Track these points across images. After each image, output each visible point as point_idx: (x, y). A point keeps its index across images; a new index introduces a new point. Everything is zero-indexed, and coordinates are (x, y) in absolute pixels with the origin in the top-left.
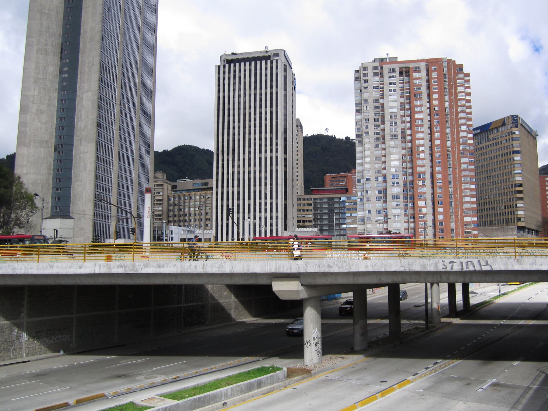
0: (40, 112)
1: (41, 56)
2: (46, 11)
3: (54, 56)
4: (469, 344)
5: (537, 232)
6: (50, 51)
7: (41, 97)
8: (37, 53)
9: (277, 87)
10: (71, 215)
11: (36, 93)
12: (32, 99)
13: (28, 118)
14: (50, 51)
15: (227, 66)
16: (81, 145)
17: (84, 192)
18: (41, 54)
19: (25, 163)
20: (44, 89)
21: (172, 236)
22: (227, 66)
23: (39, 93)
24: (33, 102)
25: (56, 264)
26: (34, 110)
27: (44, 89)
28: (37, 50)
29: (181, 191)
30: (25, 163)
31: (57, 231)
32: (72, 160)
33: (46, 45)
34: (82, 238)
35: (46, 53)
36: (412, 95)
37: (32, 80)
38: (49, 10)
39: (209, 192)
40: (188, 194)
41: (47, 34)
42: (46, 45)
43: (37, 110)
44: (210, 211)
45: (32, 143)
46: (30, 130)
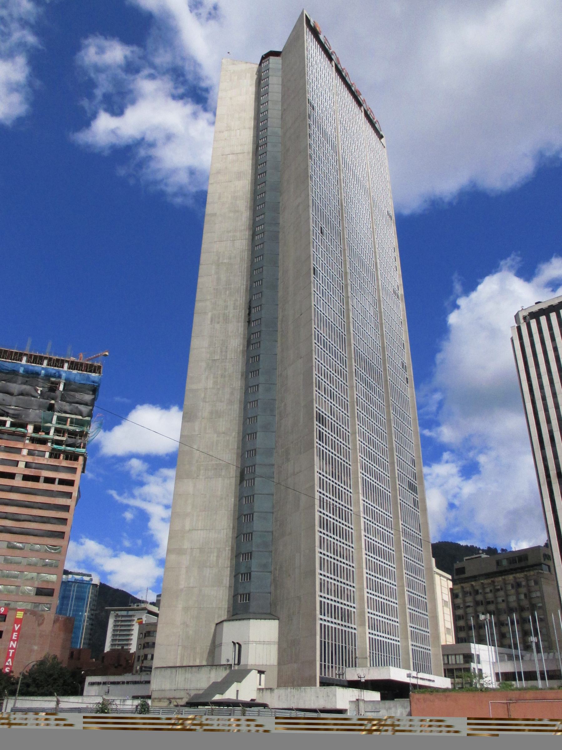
0: (216, 414)
1: (217, 326)
2: (225, 261)
3: (238, 322)
6: (231, 315)
7: (219, 389)
8: (212, 321)
9: (338, 730)
11: (210, 384)
12: (203, 395)
13: (197, 428)
14: (231, 315)
15: (533, 323)
18: (218, 323)
19: (189, 509)
20: (223, 376)
21: (480, 666)
23: (215, 383)
24: (204, 400)
26: (206, 414)
27: (223, 376)
29: (474, 578)
30: (189, 509)
31: (240, 646)
33: (226, 307)
34: (295, 666)
35: (226, 320)
37: (203, 364)
39: (532, 573)
40: (489, 581)
41: (227, 292)
42: (226, 307)
43: (211, 413)
45: (202, 472)
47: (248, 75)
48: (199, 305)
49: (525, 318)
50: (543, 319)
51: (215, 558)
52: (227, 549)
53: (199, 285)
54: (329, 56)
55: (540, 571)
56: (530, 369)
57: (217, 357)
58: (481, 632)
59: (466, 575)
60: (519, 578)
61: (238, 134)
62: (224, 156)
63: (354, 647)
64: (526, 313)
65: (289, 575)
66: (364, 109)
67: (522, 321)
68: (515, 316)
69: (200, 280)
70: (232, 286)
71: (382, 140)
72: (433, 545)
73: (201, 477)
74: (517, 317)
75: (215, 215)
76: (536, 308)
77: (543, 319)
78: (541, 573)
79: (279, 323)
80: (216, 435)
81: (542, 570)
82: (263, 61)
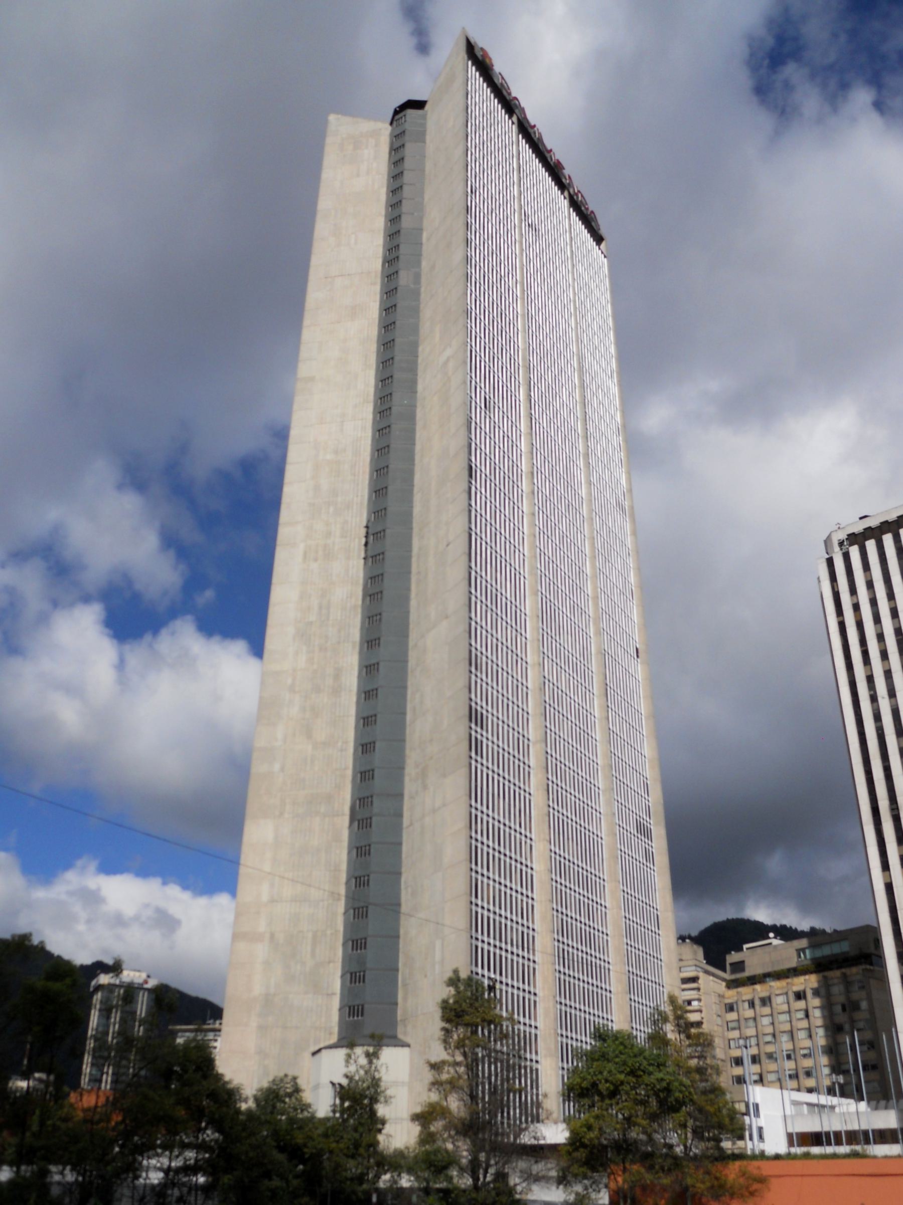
2: (329, 457)
4: (23, 1084)
5: (770, 1176)
10: (400, 1036)
12: (290, 681)
15: (854, 551)
16: (425, 787)
17: (438, 944)
18: (316, 560)
22: (854, 551)
24: (292, 689)
25: (84, 1071)
28: (305, 553)
32: (400, 844)
33: (329, 534)
36: (742, 1022)
37: (291, 630)
38: (336, 452)
41: (331, 509)
42: (329, 534)
44: (863, 994)
46: (282, 769)
47: (372, 141)
48: (284, 532)
49: (841, 544)
50: (871, 545)
51: (309, 948)
52: (329, 932)
53: (285, 499)
54: (509, 106)
55: (868, 967)
56: (848, 630)
57: (313, 618)
58: (840, 1038)
59: (747, 973)
60: (832, 978)
61: (353, 241)
62: (330, 280)
63: (535, 1090)
64: (842, 535)
65: (426, 976)
66: (519, 119)
67: (837, 548)
68: (825, 542)
69: (286, 490)
70: (339, 499)
71: (603, 245)
72: (233, 892)
73: (286, 816)
74: (827, 542)
75: (312, 379)
76: (859, 528)
77: (871, 545)
78: (870, 970)
79: (414, 560)
80: (310, 747)
81: (871, 964)
82: (397, 117)
